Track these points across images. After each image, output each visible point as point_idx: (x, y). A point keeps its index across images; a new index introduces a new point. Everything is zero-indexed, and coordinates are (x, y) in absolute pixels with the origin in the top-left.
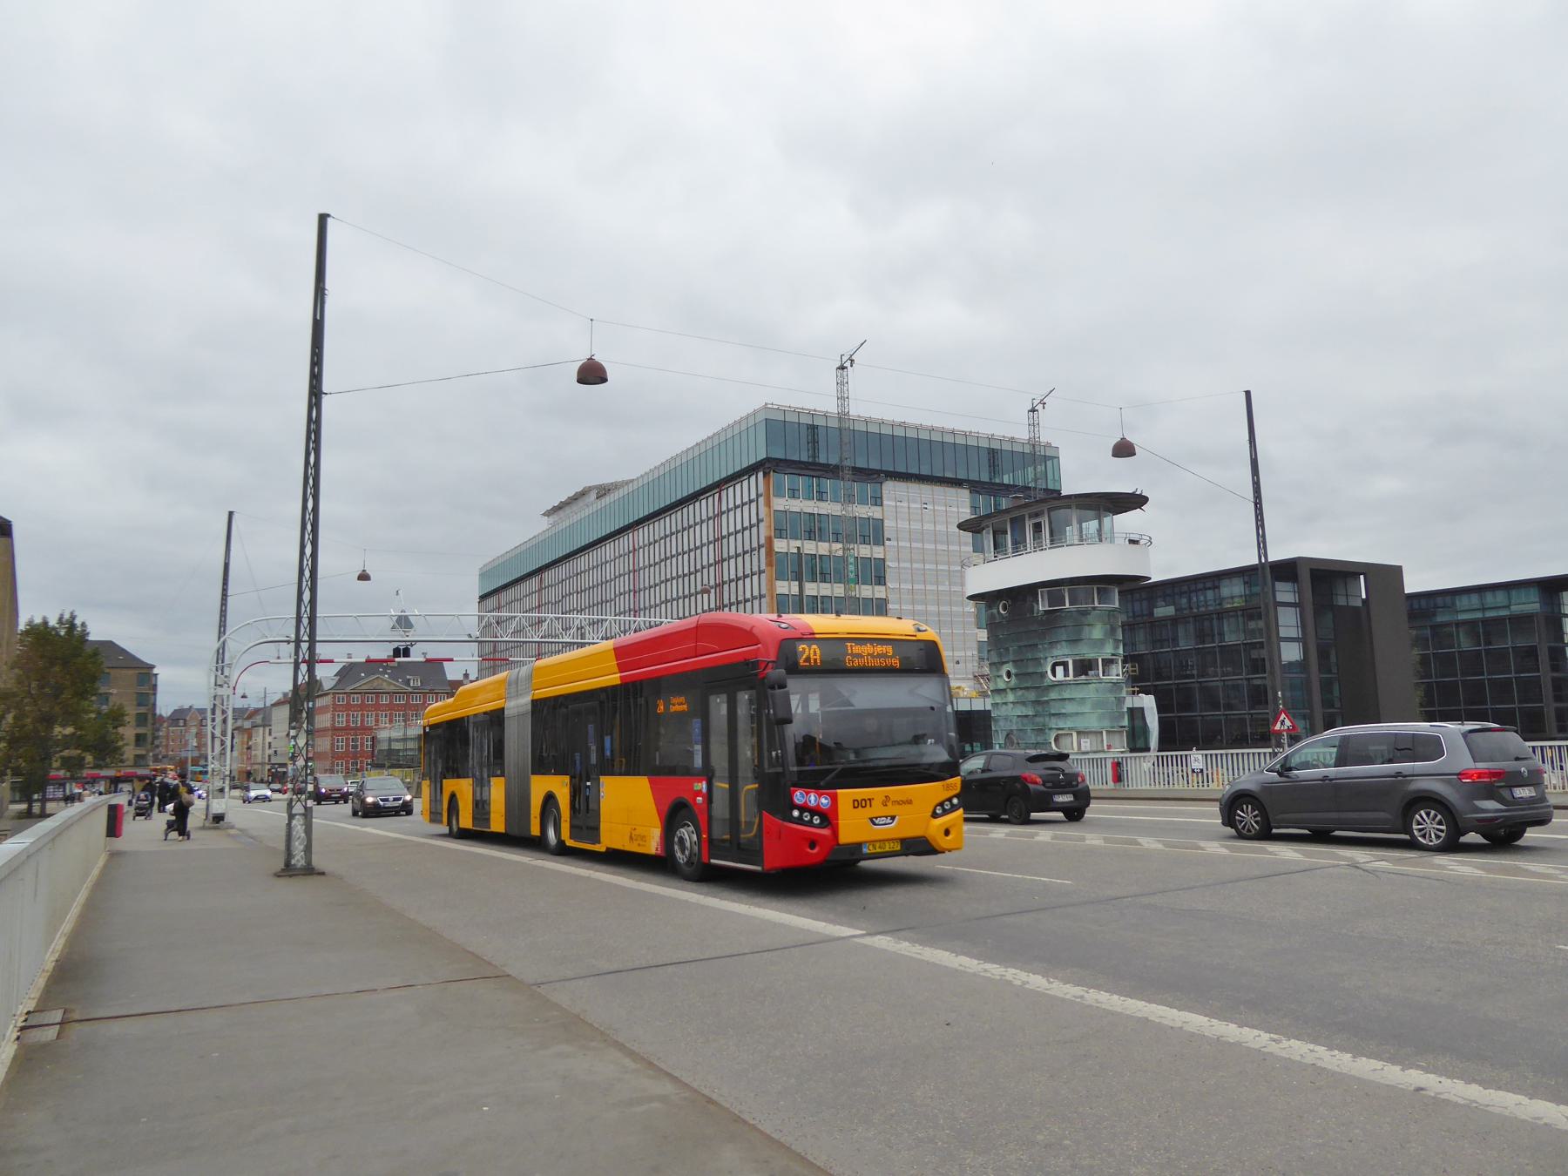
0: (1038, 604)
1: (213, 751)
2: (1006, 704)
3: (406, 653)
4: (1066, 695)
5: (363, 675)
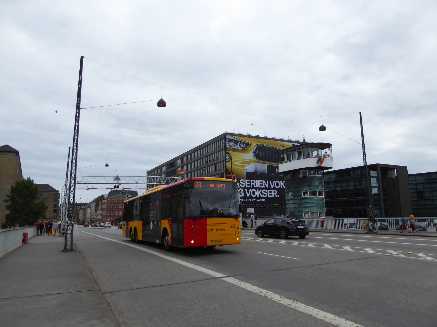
0: (299, 175)
1: (63, 214)
2: (290, 204)
3: (118, 187)
4: (308, 202)
5: (115, 194)
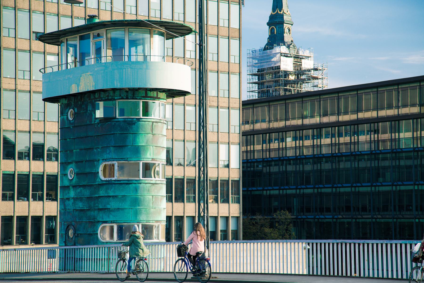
4: (111, 194)
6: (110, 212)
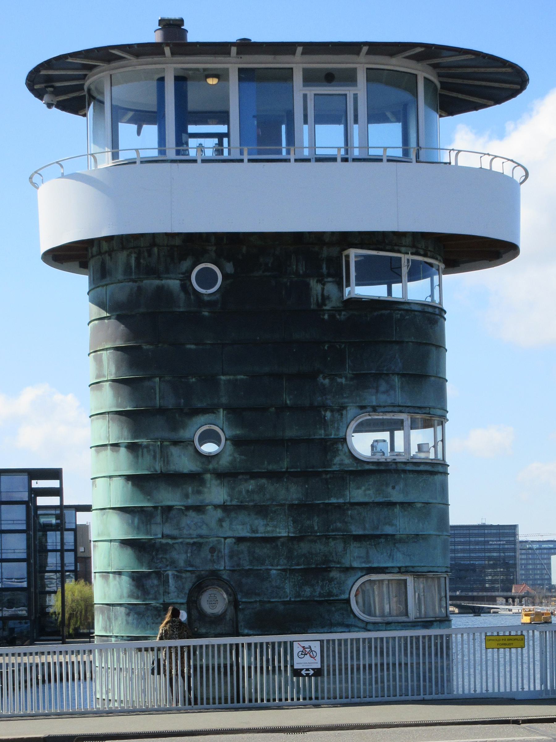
2: (199, 509)
4: (396, 496)
6: (397, 545)
